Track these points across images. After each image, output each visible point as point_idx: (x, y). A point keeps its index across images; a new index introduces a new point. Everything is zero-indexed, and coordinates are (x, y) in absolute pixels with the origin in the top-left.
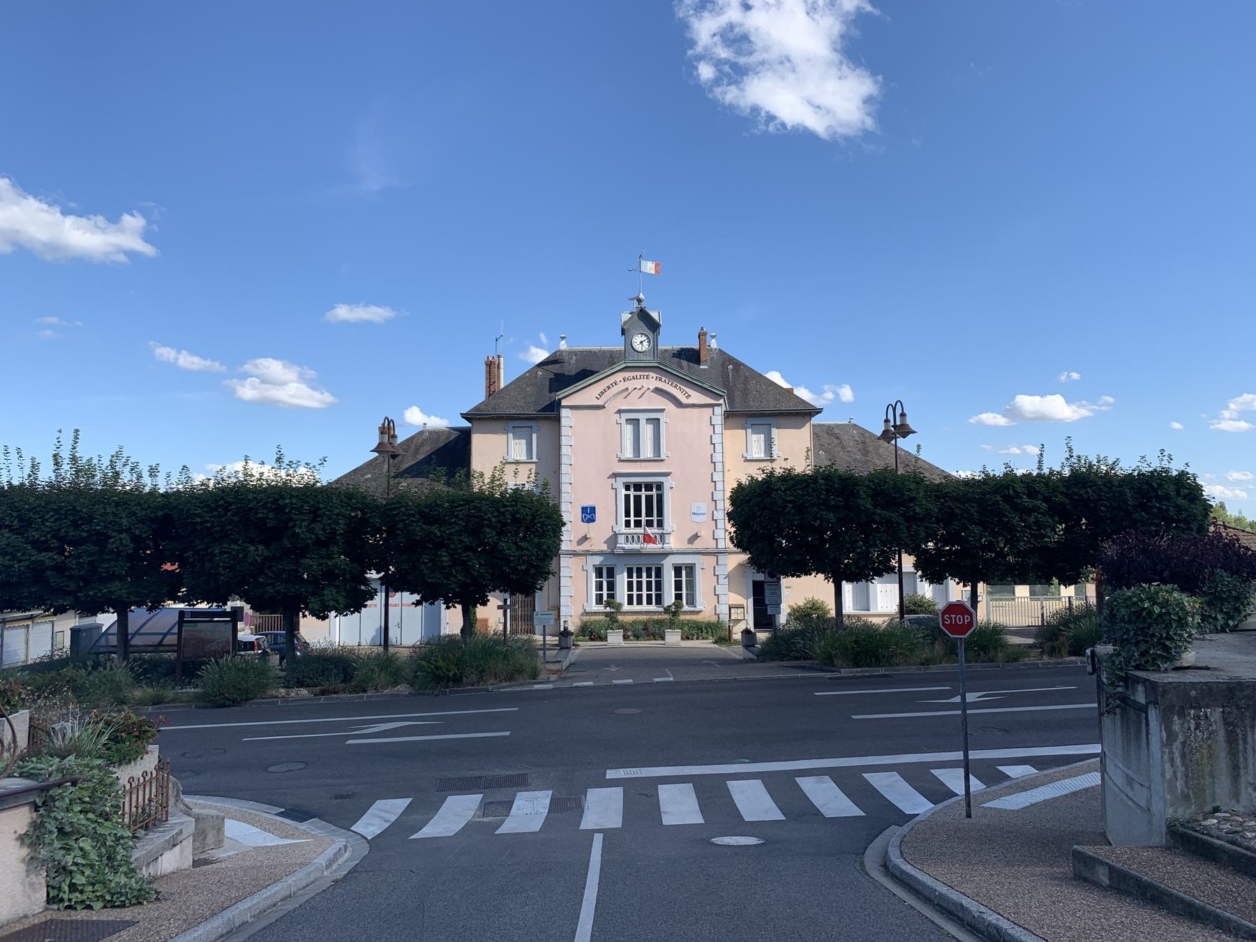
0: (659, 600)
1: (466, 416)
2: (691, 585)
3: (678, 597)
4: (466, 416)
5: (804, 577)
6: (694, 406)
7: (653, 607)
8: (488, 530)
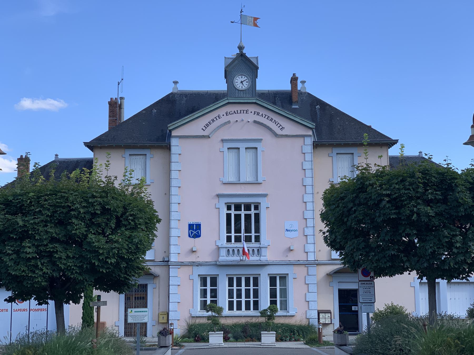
0: (256, 304)
1: (91, 146)
2: (284, 293)
3: (273, 303)
4: (91, 146)
5: (397, 276)
6: (287, 136)
7: (252, 312)
8: (74, 220)
